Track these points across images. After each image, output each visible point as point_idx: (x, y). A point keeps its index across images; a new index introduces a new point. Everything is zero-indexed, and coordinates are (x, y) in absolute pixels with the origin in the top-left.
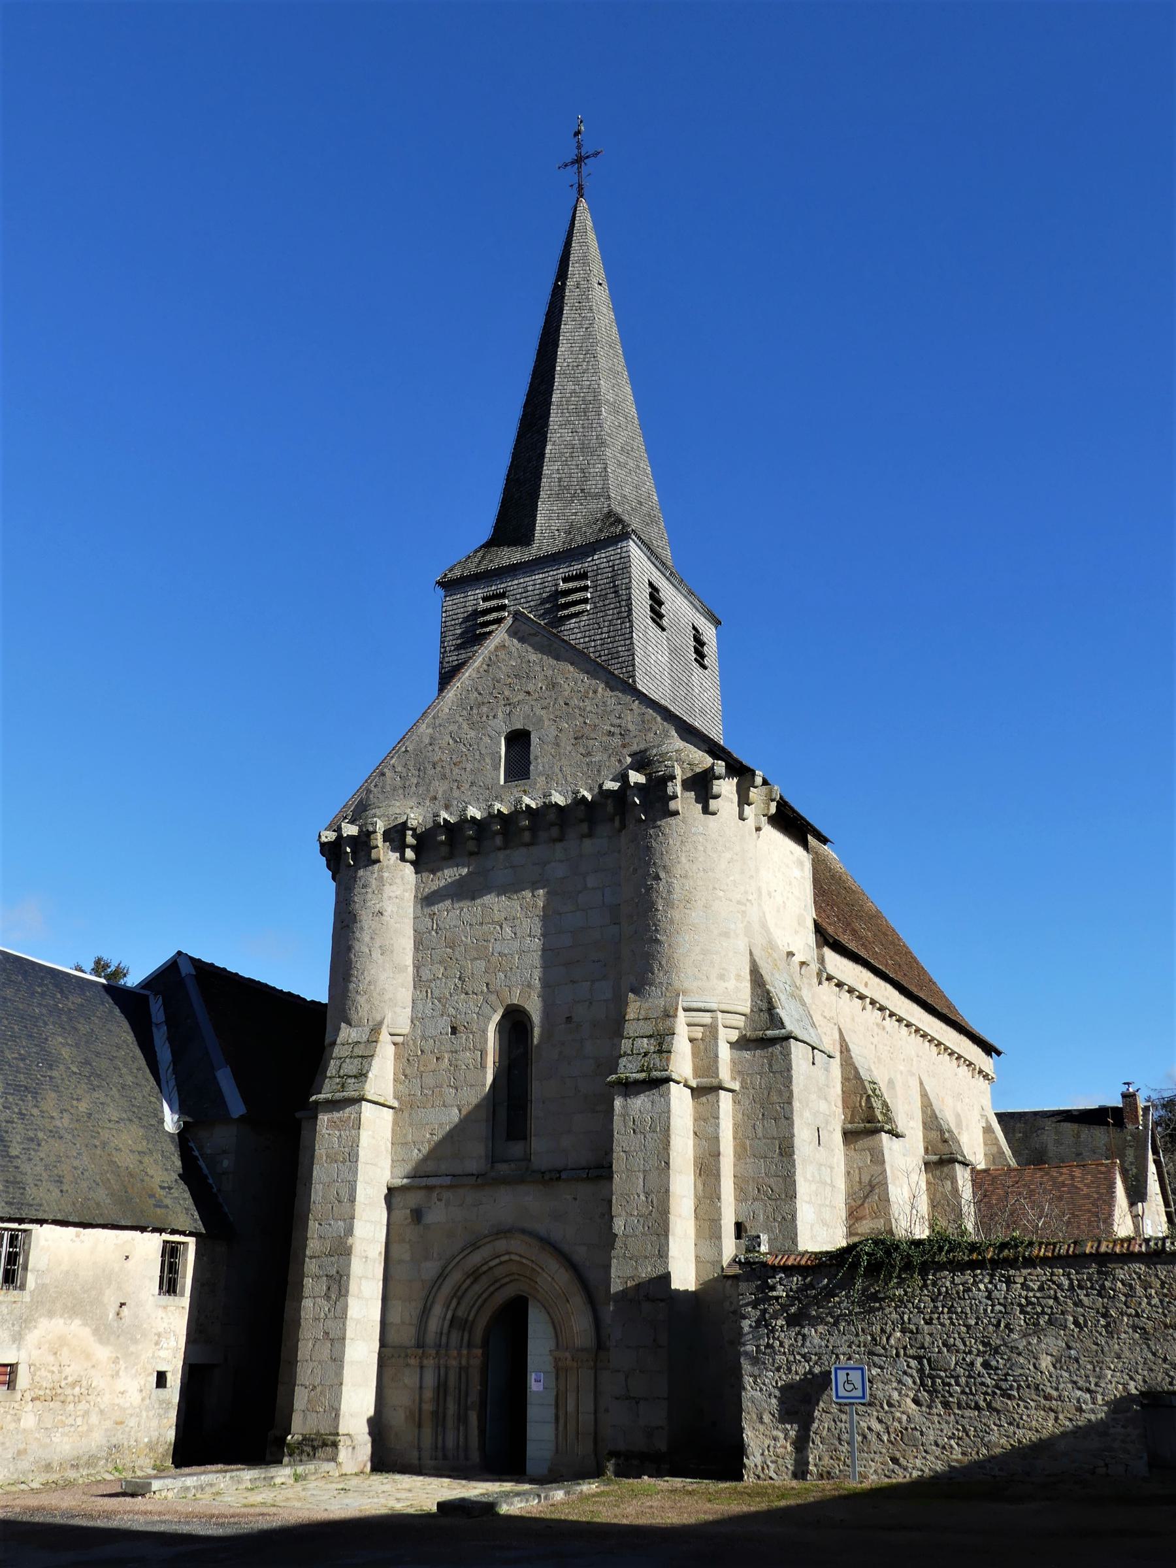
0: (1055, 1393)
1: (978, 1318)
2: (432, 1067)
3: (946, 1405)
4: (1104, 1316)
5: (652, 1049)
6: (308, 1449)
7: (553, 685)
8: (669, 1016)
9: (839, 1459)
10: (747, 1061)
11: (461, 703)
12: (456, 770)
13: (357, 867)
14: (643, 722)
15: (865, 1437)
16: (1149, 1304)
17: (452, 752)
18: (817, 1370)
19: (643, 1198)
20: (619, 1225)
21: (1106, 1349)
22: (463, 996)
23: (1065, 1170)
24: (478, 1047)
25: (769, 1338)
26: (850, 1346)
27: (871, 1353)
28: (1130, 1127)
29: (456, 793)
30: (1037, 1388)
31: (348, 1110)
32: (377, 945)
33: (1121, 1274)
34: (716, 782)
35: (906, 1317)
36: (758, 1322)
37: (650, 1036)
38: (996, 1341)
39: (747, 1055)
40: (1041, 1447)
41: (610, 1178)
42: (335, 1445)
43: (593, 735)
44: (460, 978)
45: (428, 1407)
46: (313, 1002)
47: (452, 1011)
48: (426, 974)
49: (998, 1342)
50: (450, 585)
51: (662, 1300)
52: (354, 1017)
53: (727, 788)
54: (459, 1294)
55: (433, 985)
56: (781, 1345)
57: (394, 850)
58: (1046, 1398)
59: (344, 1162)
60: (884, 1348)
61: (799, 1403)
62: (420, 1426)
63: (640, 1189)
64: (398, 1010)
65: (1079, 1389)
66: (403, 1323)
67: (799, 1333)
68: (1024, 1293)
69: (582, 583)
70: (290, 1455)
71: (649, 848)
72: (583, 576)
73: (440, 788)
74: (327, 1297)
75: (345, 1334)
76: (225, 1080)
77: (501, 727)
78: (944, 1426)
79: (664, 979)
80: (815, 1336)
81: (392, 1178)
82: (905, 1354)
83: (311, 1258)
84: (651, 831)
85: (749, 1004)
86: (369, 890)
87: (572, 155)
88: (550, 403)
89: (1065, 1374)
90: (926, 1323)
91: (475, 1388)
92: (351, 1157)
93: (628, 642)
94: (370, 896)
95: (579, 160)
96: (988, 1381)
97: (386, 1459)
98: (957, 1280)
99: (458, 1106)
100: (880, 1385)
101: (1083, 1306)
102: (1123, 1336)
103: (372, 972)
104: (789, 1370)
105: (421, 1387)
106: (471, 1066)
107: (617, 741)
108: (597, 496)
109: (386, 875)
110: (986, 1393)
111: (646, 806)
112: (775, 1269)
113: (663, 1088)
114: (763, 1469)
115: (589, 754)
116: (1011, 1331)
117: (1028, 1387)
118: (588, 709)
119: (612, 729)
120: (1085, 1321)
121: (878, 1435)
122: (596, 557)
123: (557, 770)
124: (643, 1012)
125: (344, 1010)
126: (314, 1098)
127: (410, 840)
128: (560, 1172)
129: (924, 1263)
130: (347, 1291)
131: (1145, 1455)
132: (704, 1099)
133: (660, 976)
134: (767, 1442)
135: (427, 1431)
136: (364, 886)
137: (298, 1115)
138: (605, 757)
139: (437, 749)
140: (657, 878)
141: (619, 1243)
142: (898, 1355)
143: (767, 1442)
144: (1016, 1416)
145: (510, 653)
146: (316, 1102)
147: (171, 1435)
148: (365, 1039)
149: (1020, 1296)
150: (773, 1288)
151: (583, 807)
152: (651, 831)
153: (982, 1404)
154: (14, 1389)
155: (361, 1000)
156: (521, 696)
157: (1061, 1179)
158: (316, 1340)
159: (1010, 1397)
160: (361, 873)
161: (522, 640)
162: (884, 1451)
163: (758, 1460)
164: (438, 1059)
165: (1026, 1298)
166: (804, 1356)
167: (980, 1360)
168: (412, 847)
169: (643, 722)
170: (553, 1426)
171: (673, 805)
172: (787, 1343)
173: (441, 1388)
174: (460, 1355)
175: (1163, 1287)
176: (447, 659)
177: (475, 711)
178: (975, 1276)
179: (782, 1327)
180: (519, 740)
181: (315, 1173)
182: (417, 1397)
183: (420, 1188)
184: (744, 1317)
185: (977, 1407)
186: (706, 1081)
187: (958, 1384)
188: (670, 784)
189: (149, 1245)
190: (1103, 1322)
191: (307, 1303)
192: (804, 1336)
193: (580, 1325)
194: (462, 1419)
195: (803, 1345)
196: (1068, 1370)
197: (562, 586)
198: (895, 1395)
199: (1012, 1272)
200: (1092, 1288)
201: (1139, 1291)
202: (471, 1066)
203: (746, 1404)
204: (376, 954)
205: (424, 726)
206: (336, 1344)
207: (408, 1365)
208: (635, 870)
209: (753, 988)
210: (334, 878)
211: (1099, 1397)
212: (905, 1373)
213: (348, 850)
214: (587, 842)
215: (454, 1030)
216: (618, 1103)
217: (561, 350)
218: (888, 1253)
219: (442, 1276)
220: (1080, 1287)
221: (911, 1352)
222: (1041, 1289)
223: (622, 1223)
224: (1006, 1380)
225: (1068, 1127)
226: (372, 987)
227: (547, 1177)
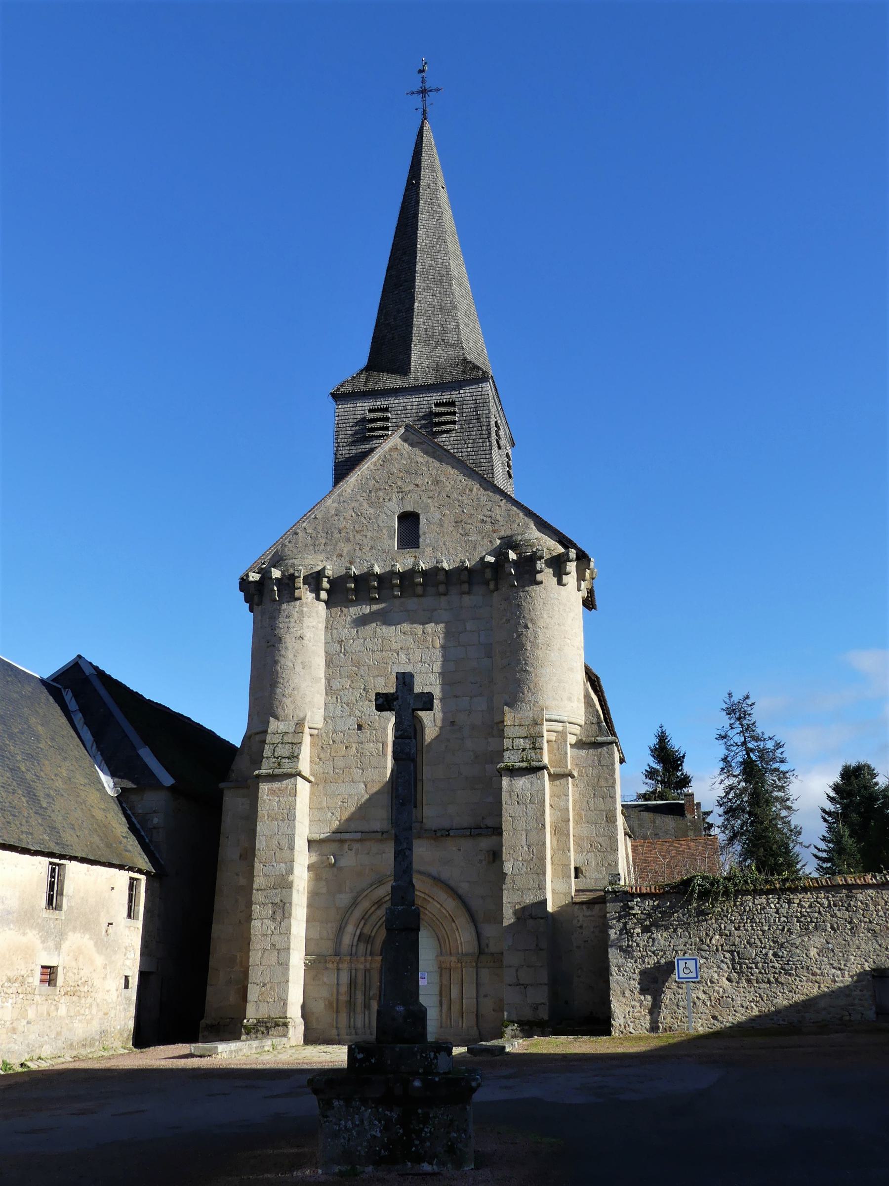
0: (819, 972)
1: (770, 926)
2: (343, 753)
3: (749, 981)
4: (850, 923)
5: (528, 746)
6: (263, 1029)
7: (437, 482)
8: (537, 724)
9: (677, 1018)
10: (582, 757)
11: (362, 487)
12: (358, 537)
13: (281, 602)
14: (509, 515)
15: (695, 1003)
16: (877, 915)
17: (354, 522)
18: (663, 961)
19: (526, 848)
20: (508, 867)
21: (851, 943)
22: (367, 702)
23: (683, 843)
24: (380, 739)
25: (628, 941)
26: (685, 945)
27: (700, 949)
28: (689, 816)
29: (358, 553)
30: (808, 969)
31: (285, 782)
32: (299, 662)
33: (860, 897)
34: (568, 563)
35: (723, 926)
36: (621, 930)
37: (526, 737)
38: (782, 940)
39: (583, 752)
40: (809, 1004)
41: (501, 834)
42: (286, 1025)
43: (469, 521)
44: (364, 689)
45: (344, 998)
46: (149, 700)
47: (358, 713)
48: (336, 685)
49: (783, 940)
50: (338, 397)
51: (542, 918)
52: (280, 712)
54: (366, 917)
55: (341, 693)
56: (638, 945)
57: (311, 591)
58: (813, 974)
59: (283, 820)
60: (708, 946)
61: (654, 981)
62: (337, 1012)
63: (524, 842)
64: (315, 710)
65: (834, 968)
66: (322, 939)
67: (650, 937)
68: (799, 910)
69: (452, 409)
70: (247, 1034)
71: (519, 606)
72: (452, 404)
73: (346, 548)
74: (273, 919)
75: (289, 945)
76: (147, 755)
77: (395, 508)
78: (747, 994)
79: (532, 699)
80: (661, 937)
81: (310, 833)
82: (722, 950)
83: (258, 890)
84: (521, 594)
85: (583, 718)
86: (292, 620)
87: (418, 86)
88: (415, 271)
89: (826, 959)
90: (736, 929)
91: (376, 983)
92: (290, 817)
93: (488, 456)
94: (292, 624)
95: (423, 92)
96: (777, 965)
97: (310, 1039)
98: (756, 902)
99: (364, 782)
100: (706, 970)
101: (836, 917)
102: (861, 935)
103: (296, 681)
104: (644, 962)
105: (338, 984)
106: (375, 754)
107: (488, 527)
108: (453, 346)
109: (305, 609)
110: (775, 973)
111: (518, 576)
112: (633, 895)
113: (539, 773)
114: (625, 1027)
115: (466, 534)
116: (791, 933)
117: (802, 968)
118: (466, 502)
119: (485, 519)
120: (838, 926)
121: (704, 1002)
122: (462, 391)
123: (441, 544)
124: (517, 720)
125: (272, 708)
126: (257, 772)
127: (325, 584)
128: (448, 831)
129: (736, 891)
130: (290, 914)
131: (874, 1008)
132: (557, 782)
133: (529, 696)
134: (628, 1009)
135: (343, 1016)
136: (288, 617)
137: (222, 785)
138: (480, 538)
139: (342, 519)
140: (526, 627)
141: (508, 880)
142: (717, 950)
143: (628, 1009)
144: (794, 986)
145: (401, 454)
146: (258, 776)
147: (131, 1024)
148: (292, 730)
149: (797, 911)
150: (632, 908)
151: (466, 573)
152: (521, 594)
153: (772, 979)
154: (55, 985)
155: (287, 701)
156: (411, 487)
157: (681, 849)
158: (265, 950)
159: (790, 975)
160: (284, 606)
161: (411, 445)
162: (707, 1012)
163: (622, 1021)
164: (346, 747)
165: (801, 912)
166: (653, 953)
167: (771, 952)
168: (326, 590)
169: (509, 515)
170: (438, 1009)
171: (539, 577)
172: (642, 944)
173: (352, 984)
174: (366, 960)
175: (886, 905)
176: (340, 452)
177: (373, 494)
178: (769, 899)
179: (638, 934)
181: (258, 828)
182: (335, 991)
183: (334, 841)
184: (611, 928)
185: (769, 982)
186: (559, 770)
187: (757, 968)
188: (538, 562)
189: (122, 878)
190: (849, 927)
191: (256, 924)
192: (654, 939)
193: (463, 937)
194: (367, 1006)
195: (653, 945)
196: (827, 957)
197: (435, 409)
198: (716, 976)
199: (792, 896)
200: (842, 906)
201: (872, 907)
202: (375, 754)
203: (613, 985)
204: (298, 668)
205: (330, 501)
206: (283, 954)
207: (327, 968)
208: (508, 621)
209: (586, 708)
210: (251, 610)
211: (846, 973)
212: (722, 961)
213: (275, 588)
214: (466, 598)
215: (360, 727)
216: (505, 782)
217: (420, 232)
218: (712, 884)
219: (354, 903)
220: (835, 905)
221: (726, 948)
222: (810, 907)
223: (510, 866)
224: (788, 964)
225: (645, 815)
226: (296, 692)
227: (438, 834)
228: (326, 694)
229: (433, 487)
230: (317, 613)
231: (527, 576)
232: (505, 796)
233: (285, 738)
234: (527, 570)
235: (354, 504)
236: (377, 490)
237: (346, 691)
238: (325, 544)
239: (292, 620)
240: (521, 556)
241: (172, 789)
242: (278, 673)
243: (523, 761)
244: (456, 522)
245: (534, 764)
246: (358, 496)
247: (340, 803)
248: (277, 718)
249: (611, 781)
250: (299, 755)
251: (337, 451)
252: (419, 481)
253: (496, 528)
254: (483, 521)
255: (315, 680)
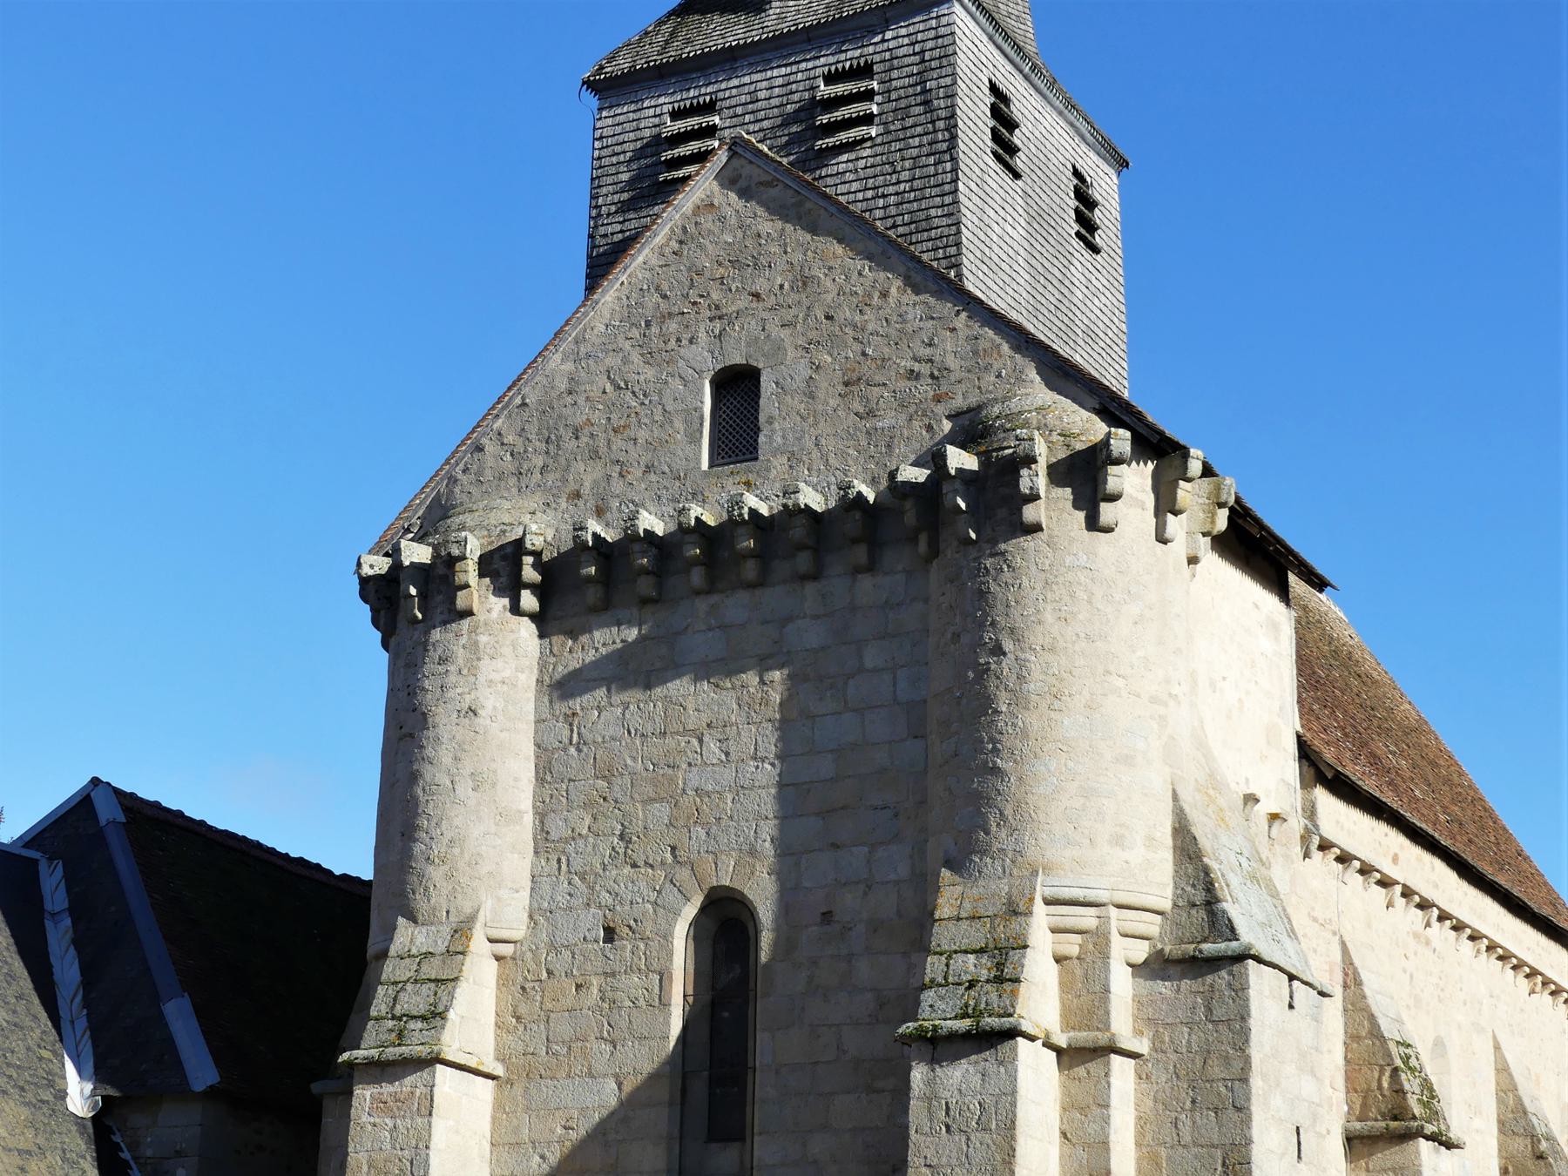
7: (804, 281)
12: (618, 443)
13: (428, 624)
17: (610, 407)
22: (627, 870)
29: (617, 486)
31: (409, 1080)
32: (467, 771)
34: (1112, 469)
37: (981, 951)
39: (1164, 988)
43: (879, 378)
44: (622, 837)
46: (345, 877)
47: (606, 898)
48: (558, 829)
50: (609, 88)
52: (421, 905)
53: (1133, 481)
55: (570, 849)
64: (504, 893)
69: (862, 85)
71: (982, 595)
72: (865, 71)
73: (588, 475)
77: (703, 360)
79: (1009, 845)
84: (989, 562)
86: (452, 668)
93: (948, 199)
94: (452, 678)
99: (616, 1076)
103: (457, 822)
106: (642, 1003)
107: (925, 389)
109: (483, 639)
111: (977, 513)
113: (1005, 1047)
115: (871, 414)
118: (870, 327)
122: (889, 35)
123: (809, 443)
124: (967, 905)
126: (345, 1056)
127: (529, 573)
132: (1081, 1071)
133: (1001, 838)
136: (443, 661)
139: (581, 401)
140: (998, 651)
145: (722, 219)
146: (350, 1065)
148: (442, 948)
151: (858, 515)
152: (989, 562)
155: (436, 874)
156: (743, 302)
160: (436, 634)
161: (745, 194)
164: (578, 987)
168: (532, 587)
169: (975, 353)
171: (1030, 513)
176: (602, 230)
177: (654, 329)
180: (737, 386)
186: (1084, 1037)
197: (824, 90)
202: (642, 1003)
204: (464, 789)
205: (558, 357)
208: (956, 637)
209: (1178, 864)
213: (413, 591)
214: (866, 582)
215: (610, 934)
226: (456, 851)
228: (536, 852)
229: (794, 297)
230: (514, 646)
231: (1002, 513)
232: (917, 1112)
233: (425, 967)
234: (998, 500)
235: (612, 361)
236: (666, 317)
237: (581, 842)
238: (544, 469)
239: (452, 668)
240: (989, 458)
241: (211, 1093)
242: (417, 805)
243: (965, 1016)
244: (846, 384)
245: (990, 1022)
246: (621, 339)
247: (559, 1131)
248: (413, 918)
249: (1237, 1065)
250: (447, 1009)
251: (596, 227)
252: (761, 285)
253: (944, 389)
254: (913, 375)
255: (506, 817)
